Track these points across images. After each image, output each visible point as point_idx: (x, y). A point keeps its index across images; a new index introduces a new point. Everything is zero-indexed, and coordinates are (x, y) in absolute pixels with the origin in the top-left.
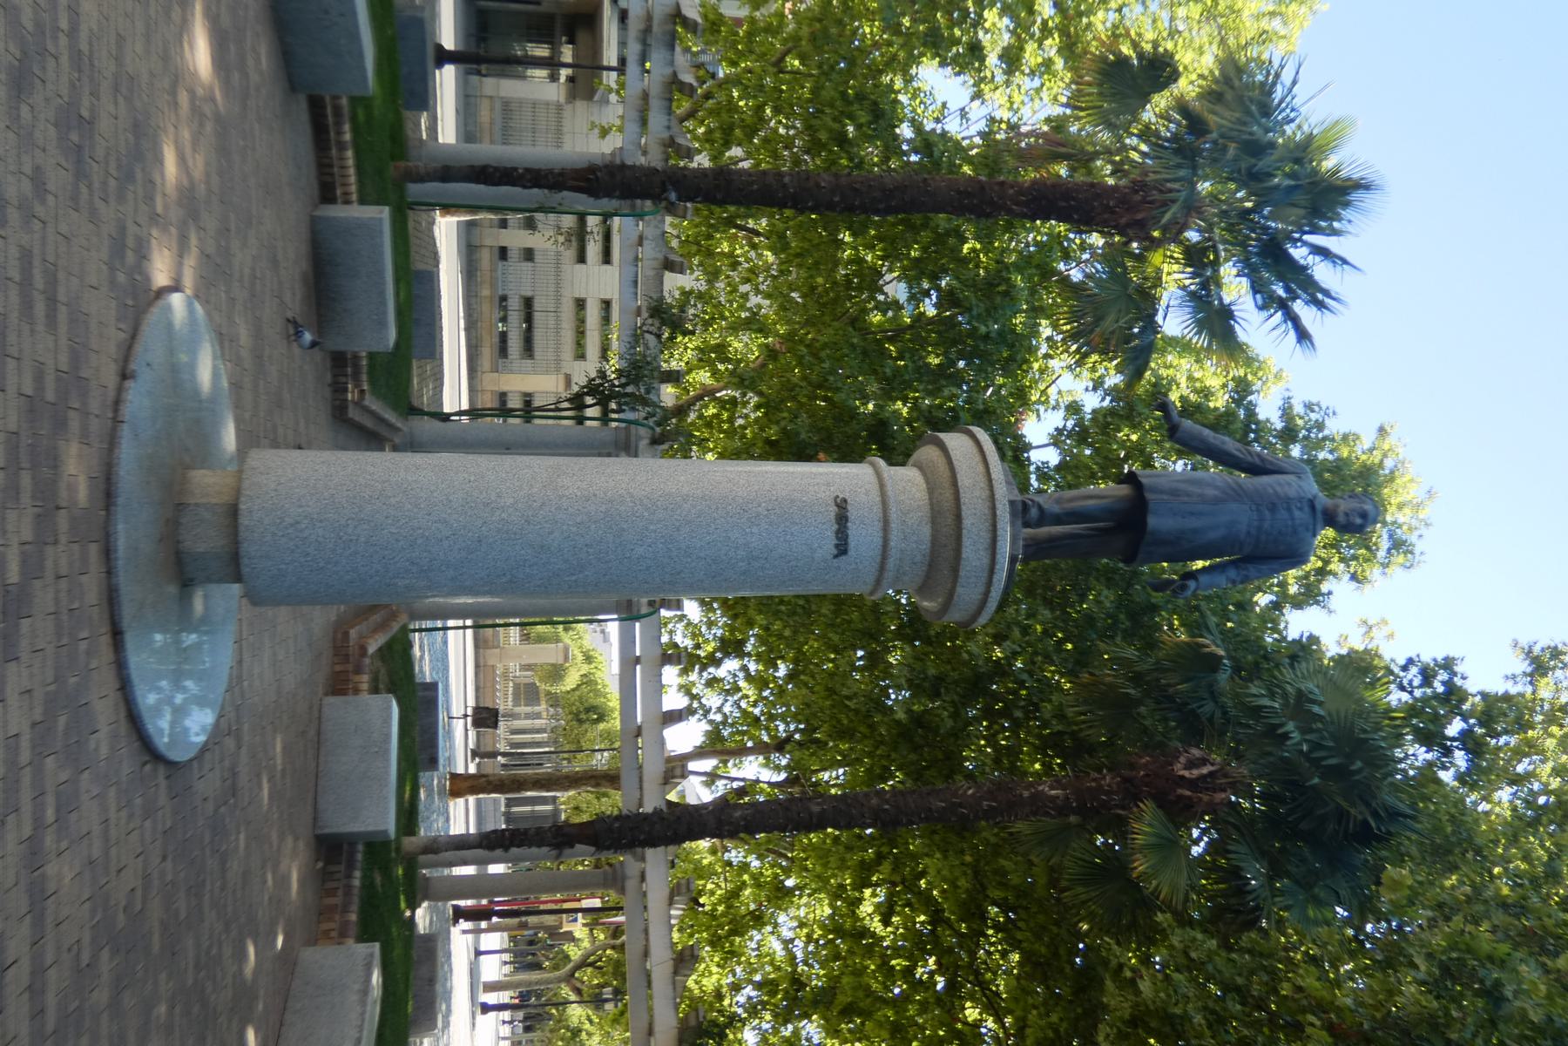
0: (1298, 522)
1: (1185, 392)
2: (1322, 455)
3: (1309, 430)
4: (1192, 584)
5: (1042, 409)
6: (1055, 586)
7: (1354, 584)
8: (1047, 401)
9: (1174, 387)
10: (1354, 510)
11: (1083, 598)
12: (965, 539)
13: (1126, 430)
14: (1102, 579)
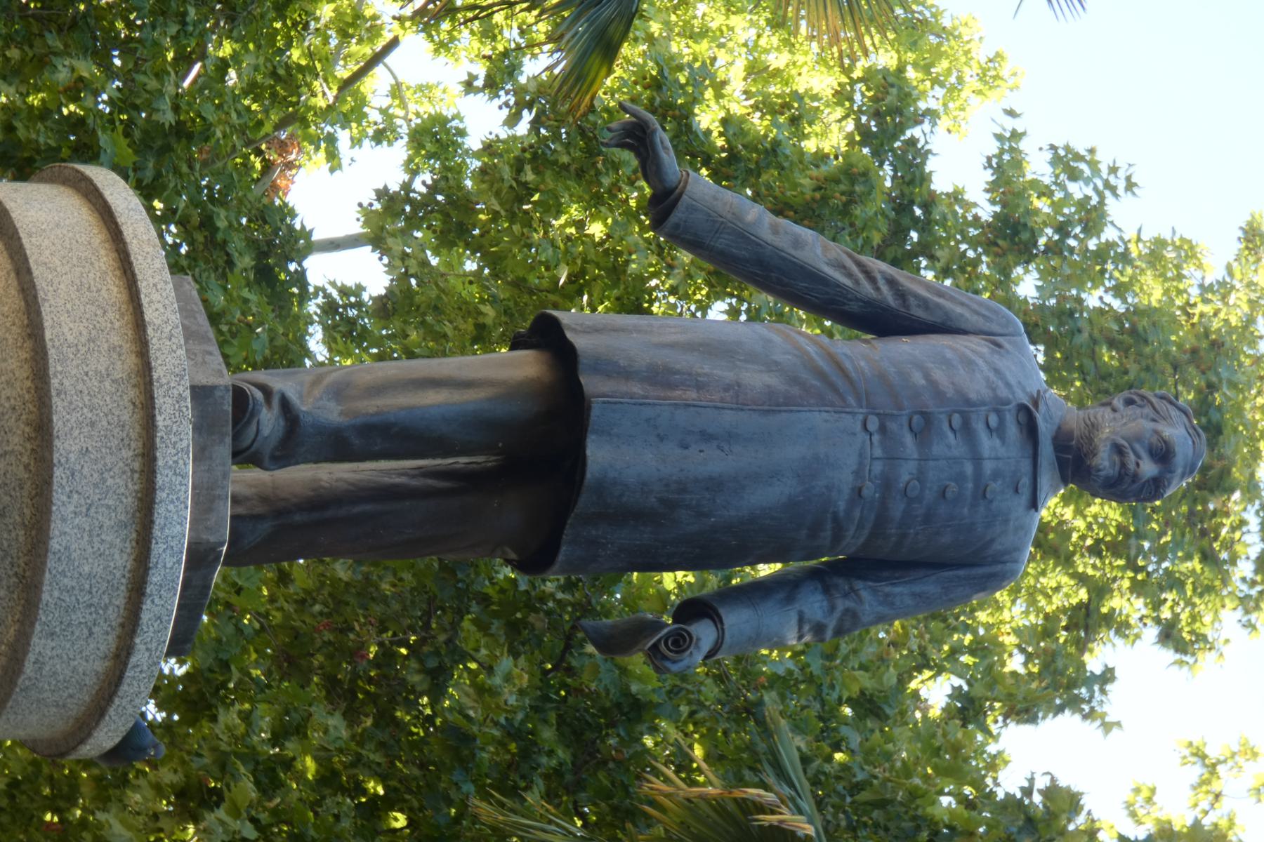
0: (988, 467)
1: (739, 107)
2: (1093, 298)
3: (1063, 230)
4: (704, 633)
5: (343, 137)
6: (363, 646)
7: (1169, 655)
8: (356, 114)
9: (709, 94)
10: (1139, 438)
11: (437, 682)
12: (59, 496)
13: (575, 211)
14: (496, 626)
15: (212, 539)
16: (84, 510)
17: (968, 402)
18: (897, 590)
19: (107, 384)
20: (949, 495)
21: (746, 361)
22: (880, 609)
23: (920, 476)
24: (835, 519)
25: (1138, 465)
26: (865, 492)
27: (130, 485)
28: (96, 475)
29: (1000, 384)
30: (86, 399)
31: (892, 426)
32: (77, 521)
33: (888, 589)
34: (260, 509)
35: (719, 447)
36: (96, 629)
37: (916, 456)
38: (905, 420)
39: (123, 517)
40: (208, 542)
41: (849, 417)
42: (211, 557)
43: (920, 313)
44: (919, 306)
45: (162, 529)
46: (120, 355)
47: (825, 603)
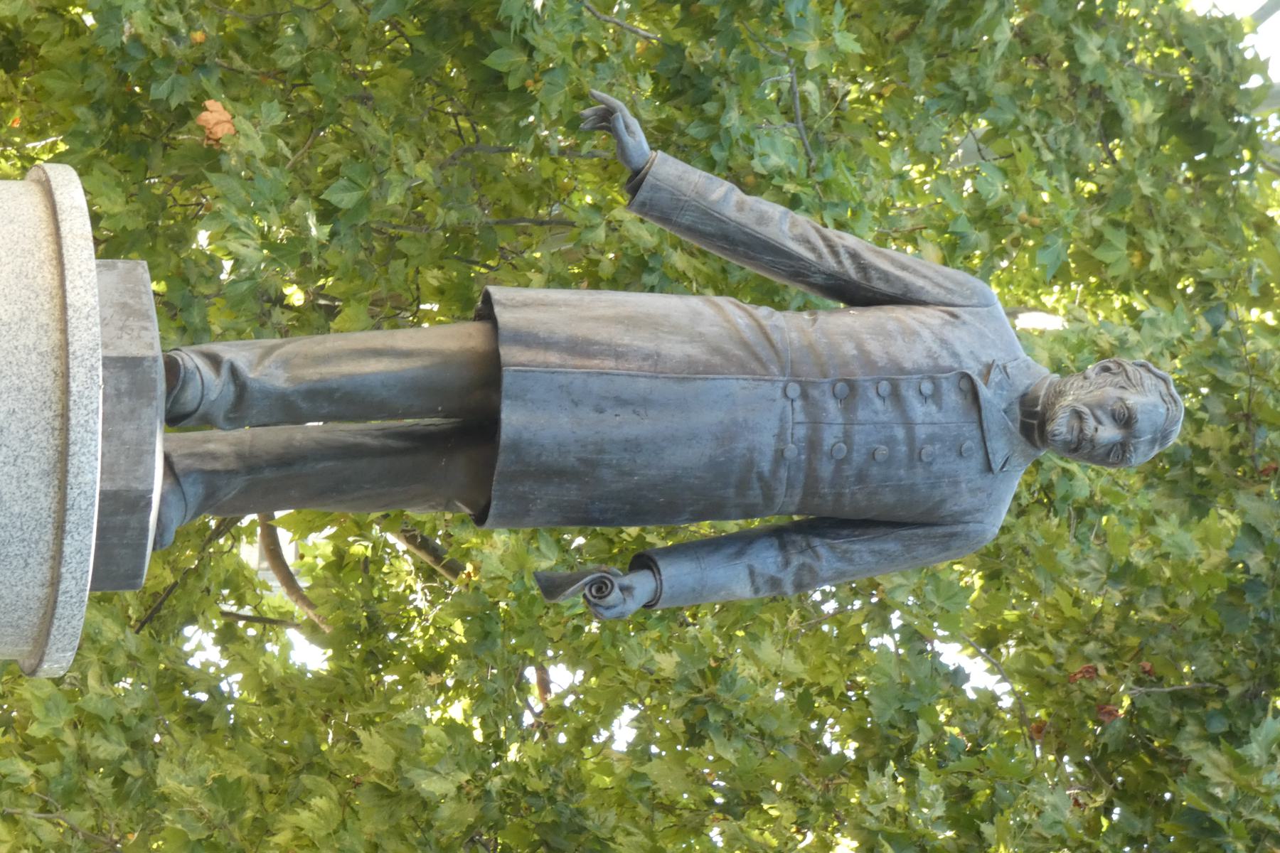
0: (922, 432)
15: (141, 487)
16: (12, 460)
17: (902, 371)
18: (856, 547)
19: (34, 356)
20: (879, 456)
21: (671, 333)
22: (838, 565)
23: (847, 438)
24: (761, 477)
25: (1096, 430)
26: (788, 454)
27: (51, 440)
28: (21, 432)
29: (944, 353)
30: (15, 369)
31: (815, 393)
32: (6, 469)
33: (845, 547)
34: (233, 465)
35: (634, 412)
36: (30, 561)
37: (840, 420)
38: (827, 387)
39: (46, 467)
40: (137, 490)
41: (768, 384)
42: (143, 504)
43: (880, 285)
44: (879, 279)
45: (76, 477)
46: (46, 332)
47: (779, 559)
